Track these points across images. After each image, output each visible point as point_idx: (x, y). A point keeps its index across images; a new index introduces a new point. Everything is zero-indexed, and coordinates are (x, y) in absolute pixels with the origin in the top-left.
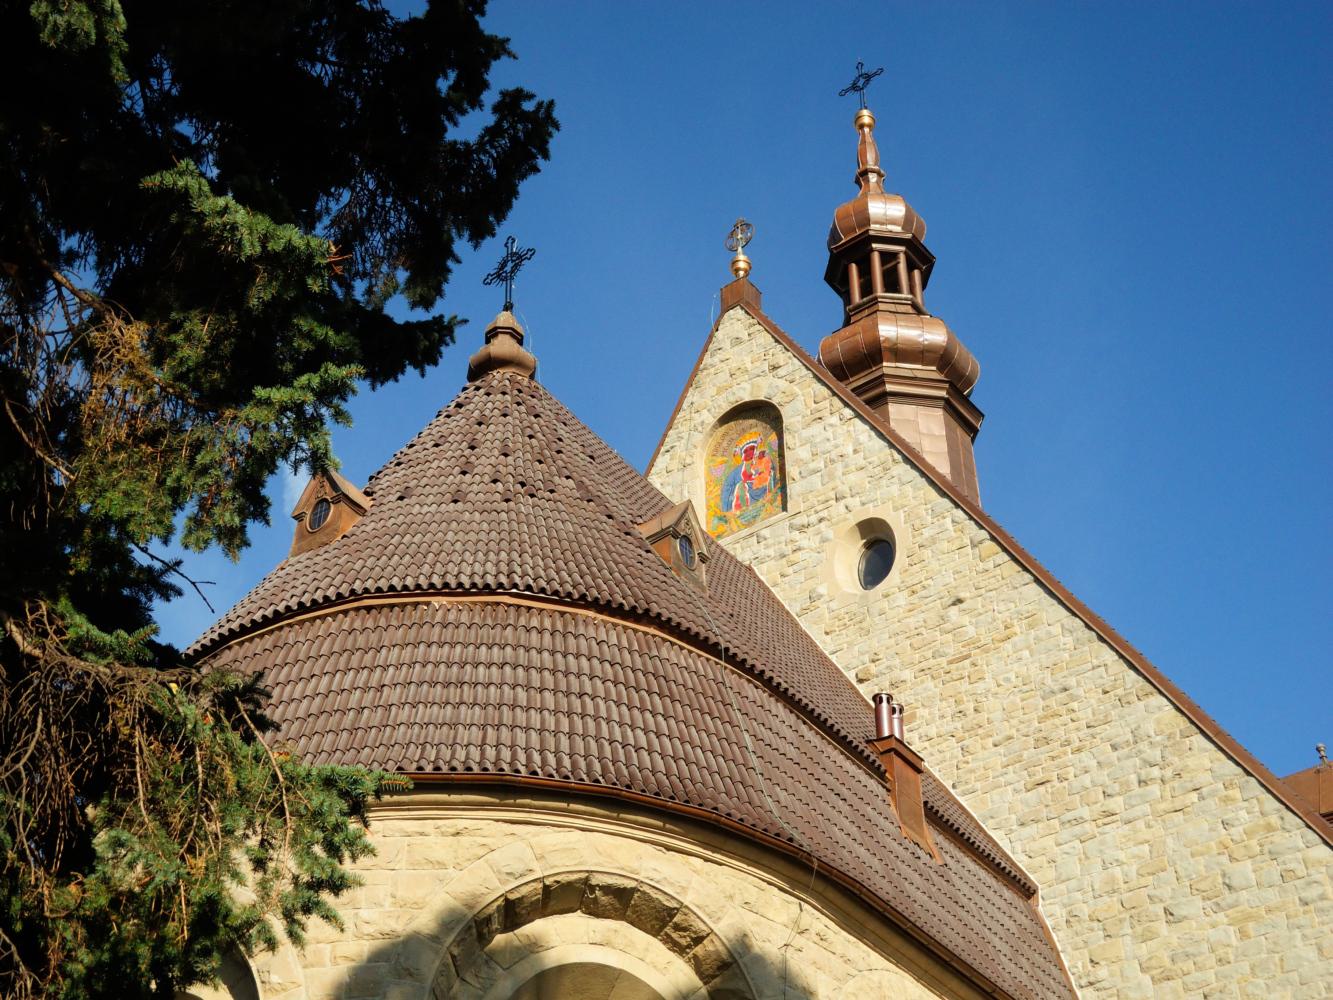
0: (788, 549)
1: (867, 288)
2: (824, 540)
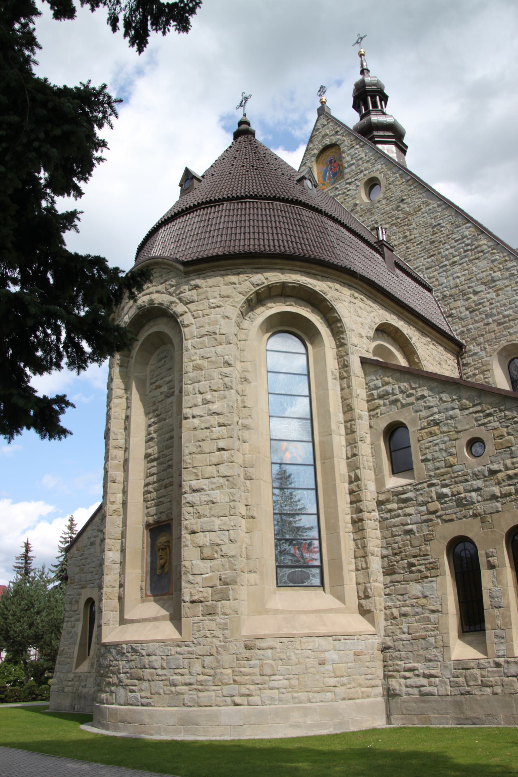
0: (345, 191)
1: (367, 108)
2: (358, 186)
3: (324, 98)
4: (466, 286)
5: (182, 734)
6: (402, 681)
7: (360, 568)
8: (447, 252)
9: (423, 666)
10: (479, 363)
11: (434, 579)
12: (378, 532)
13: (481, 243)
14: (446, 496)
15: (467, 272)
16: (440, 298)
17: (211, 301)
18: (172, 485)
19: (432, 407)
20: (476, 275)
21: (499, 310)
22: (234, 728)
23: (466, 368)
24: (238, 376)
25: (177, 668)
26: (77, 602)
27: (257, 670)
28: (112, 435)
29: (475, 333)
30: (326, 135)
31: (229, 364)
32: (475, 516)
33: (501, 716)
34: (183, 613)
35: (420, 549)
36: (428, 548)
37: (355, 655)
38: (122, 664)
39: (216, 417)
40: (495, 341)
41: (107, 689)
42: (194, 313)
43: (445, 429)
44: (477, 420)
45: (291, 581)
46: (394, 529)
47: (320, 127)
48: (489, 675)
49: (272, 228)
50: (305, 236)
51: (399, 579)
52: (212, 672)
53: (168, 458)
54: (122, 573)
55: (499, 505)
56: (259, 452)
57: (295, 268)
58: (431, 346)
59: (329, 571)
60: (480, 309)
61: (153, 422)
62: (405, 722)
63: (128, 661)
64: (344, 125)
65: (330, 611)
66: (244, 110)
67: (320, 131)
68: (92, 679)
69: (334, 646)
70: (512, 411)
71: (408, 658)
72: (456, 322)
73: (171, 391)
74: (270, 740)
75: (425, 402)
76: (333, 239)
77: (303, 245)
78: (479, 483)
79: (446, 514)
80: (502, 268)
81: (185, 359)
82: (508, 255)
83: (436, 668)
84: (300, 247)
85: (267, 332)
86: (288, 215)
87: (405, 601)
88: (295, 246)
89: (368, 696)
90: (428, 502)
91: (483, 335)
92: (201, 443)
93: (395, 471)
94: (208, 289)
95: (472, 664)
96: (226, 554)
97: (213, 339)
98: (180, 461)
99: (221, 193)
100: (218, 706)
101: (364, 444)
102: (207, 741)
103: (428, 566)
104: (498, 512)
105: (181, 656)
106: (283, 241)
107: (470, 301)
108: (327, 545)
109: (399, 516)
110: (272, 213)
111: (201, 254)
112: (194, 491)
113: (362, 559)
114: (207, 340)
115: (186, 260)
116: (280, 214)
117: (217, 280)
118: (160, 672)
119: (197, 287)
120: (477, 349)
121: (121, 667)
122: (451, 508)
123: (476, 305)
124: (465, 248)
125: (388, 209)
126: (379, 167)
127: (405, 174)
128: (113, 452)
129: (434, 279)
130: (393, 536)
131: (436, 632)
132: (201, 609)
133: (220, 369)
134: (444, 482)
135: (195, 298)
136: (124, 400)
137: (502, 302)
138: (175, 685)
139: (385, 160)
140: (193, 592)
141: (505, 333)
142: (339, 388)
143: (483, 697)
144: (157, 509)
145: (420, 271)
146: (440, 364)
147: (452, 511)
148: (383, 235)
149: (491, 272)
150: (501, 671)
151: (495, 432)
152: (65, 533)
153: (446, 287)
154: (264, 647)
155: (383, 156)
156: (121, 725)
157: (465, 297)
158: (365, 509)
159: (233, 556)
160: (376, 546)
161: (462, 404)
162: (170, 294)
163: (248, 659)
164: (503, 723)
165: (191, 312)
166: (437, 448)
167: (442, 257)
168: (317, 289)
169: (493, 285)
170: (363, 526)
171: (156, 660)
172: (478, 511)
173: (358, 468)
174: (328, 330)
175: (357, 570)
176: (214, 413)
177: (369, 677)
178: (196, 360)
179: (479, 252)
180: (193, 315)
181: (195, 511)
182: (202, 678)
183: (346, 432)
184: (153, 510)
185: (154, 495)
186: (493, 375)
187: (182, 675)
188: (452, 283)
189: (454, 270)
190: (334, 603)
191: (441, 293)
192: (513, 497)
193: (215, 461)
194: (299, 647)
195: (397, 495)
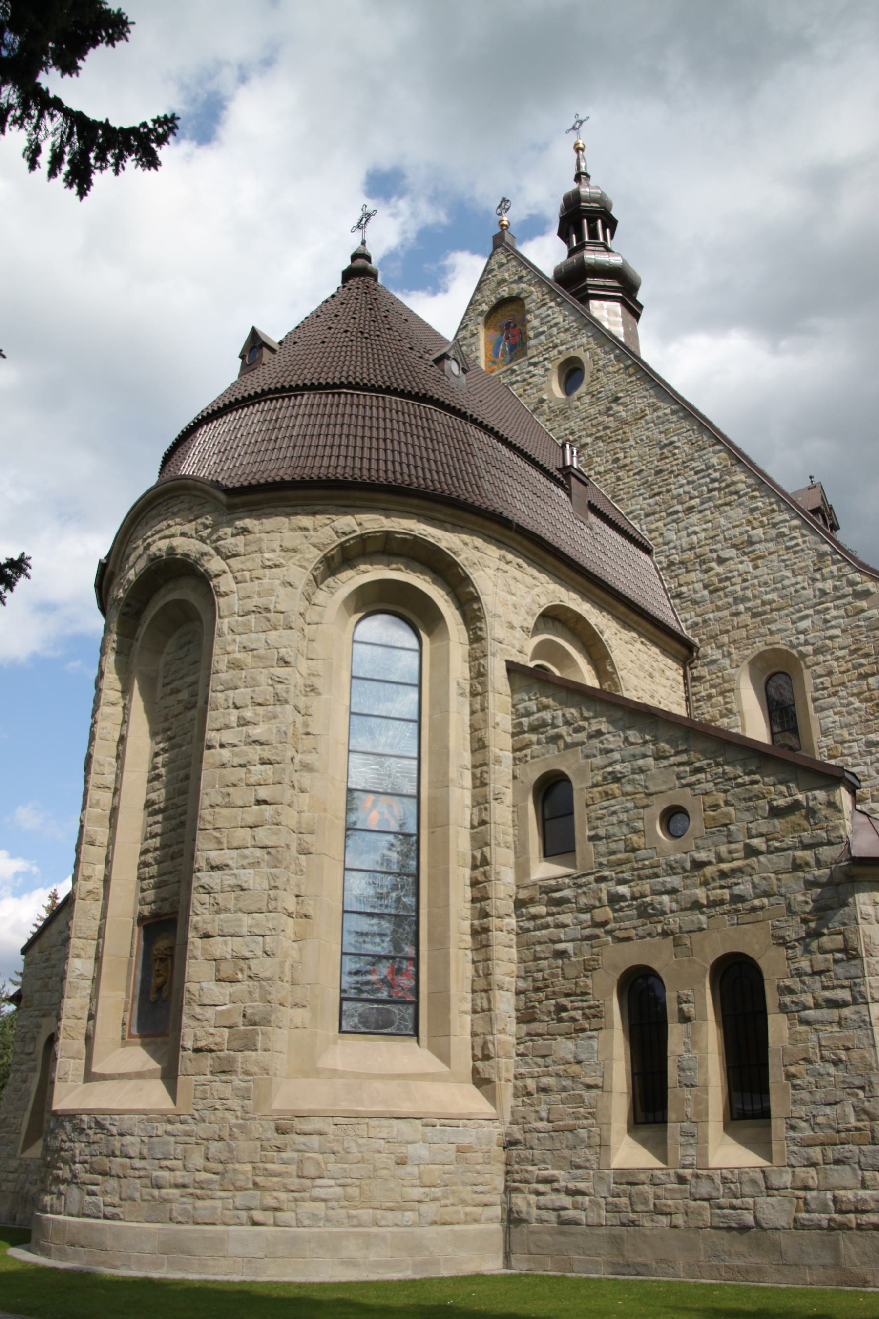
0: (527, 376)
2: (547, 370)
3: (505, 219)
4: (707, 548)
5: (165, 1268)
6: (533, 1198)
7: (479, 1009)
8: (681, 491)
9: (567, 1176)
10: (718, 677)
12: (514, 950)
13: (735, 478)
14: (622, 898)
15: (710, 524)
16: (665, 565)
17: (266, 555)
19: (612, 751)
20: (723, 531)
21: (756, 592)
22: (249, 1262)
23: (697, 684)
24: (301, 682)
25: (165, 1159)
26: (34, 1038)
27: (292, 1168)
28: (94, 766)
29: (716, 627)
30: (504, 281)
31: (286, 663)
32: (665, 934)
33: (681, 1263)
34: (181, 1068)
36: (589, 982)
38: (79, 1146)
39: (258, 748)
41: (54, 1189)
43: (629, 788)
44: (679, 778)
46: (538, 948)
47: (496, 267)
48: (667, 1196)
49: (378, 439)
50: (432, 457)
51: (540, 1031)
52: (220, 1167)
53: (180, 810)
54: (94, 996)
55: (703, 918)
56: (325, 810)
57: (408, 509)
58: (638, 646)
59: (429, 1011)
60: (725, 587)
61: (162, 749)
62: (533, 1266)
63: (89, 1143)
66: (364, 235)
67: (495, 273)
69: (424, 1135)
70: (734, 766)
71: (544, 1162)
72: (687, 607)
74: (300, 1285)
75: (602, 742)
76: (480, 463)
77: (427, 471)
78: (675, 881)
79: (620, 929)
80: (766, 522)
81: (216, 650)
82: (777, 502)
83: (586, 1180)
84: (420, 474)
85: (356, 611)
86: (407, 420)
87: (547, 1067)
89: (476, 1221)
90: (595, 907)
91: (727, 632)
92: (231, 790)
93: (549, 853)
94: (264, 536)
95: (642, 1177)
96: (257, 975)
97: (263, 620)
98: (195, 818)
99: (302, 377)
100: (225, 1224)
101: (501, 806)
102: (199, 1281)
103: (587, 1011)
104: (701, 929)
105: (172, 1139)
107: (712, 573)
108: (429, 969)
109: (547, 926)
110: (381, 415)
111: (257, 477)
112: (213, 868)
113: (483, 994)
114: (253, 621)
115: (231, 486)
116: (395, 416)
118: (137, 1163)
119: (245, 531)
120: (717, 654)
121: (77, 1152)
123: (720, 581)
125: (592, 411)
126: (584, 340)
127: (624, 356)
128: (94, 794)
129: (656, 534)
130: (537, 959)
132: (210, 1062)
133: (271, 670)
135: (241, 549)
136: (119, 709)
137: (762, 579)
138: (159, 1187)
139: (595, 330)
140: (198, 1034)
143: (655, 1232)
144: (156, 894)
145: (635, 518)
146: (651, 676)
147: (631, 924)
148: (572, 457)
149: (749, 528)
150: (685, 1191)
151: (706, 798)
153: (675, 548)
154: (307, 1131)
156: (70, 1249)
157: (704, 567)
158: (493, 913)
159: (268, 979)
160: (509, 975)
161: (658, 750)
162: (202, 540)
163: (279, 1149)
164: (682, 1274)
165: (231, 571)
166: (614, 819)
167: (673, 498)
168: (443, 545)
169: (750, 549)
170: (488, 940)
171: (133, 1144)
173: (487, 844)
174: (457, 614)
175: (474, 1011)
176: (255, 741)
177: (479, 1188)
178: (234, 652)
179: (731, 494)
180: (235, 578)
181: (212, 901)
182: (203, 1176)
183: (473, 783)
184: (150, 895)
185: (154, 869)
186: (739, 700)
187: (172, 1170)
188: (685, 541)
189: (690, 521)
191: (667, 557)
192: (726, 907)
193: (250, 820)
194: (365, 1134)
195: (547, 893)
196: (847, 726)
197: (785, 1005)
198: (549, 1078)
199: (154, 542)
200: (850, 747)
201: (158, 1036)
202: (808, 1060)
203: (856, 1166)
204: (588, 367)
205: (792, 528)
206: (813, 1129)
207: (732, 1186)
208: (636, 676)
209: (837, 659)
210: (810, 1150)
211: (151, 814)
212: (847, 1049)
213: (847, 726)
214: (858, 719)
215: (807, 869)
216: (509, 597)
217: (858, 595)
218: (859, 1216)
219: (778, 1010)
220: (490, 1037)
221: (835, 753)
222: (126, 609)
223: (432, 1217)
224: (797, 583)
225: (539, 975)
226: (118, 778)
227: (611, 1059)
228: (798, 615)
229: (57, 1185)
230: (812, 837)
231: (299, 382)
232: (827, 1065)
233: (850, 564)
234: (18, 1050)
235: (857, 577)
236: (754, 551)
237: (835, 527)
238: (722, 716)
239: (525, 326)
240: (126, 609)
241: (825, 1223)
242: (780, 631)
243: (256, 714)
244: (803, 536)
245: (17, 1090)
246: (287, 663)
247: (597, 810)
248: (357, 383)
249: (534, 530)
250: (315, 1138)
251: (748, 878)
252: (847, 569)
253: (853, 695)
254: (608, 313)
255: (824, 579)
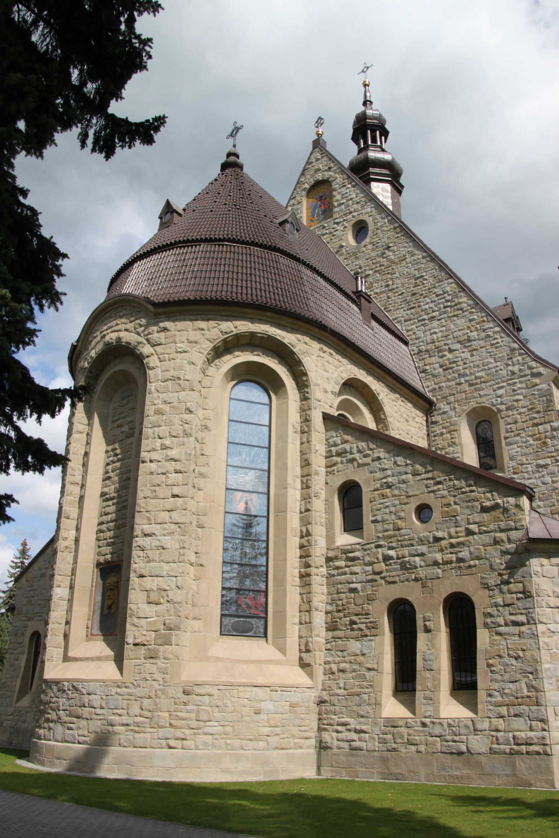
0: (333, 230)
1: (365, 142)
2: (345, 227)
3: (320, 130)
4: (442, 343)
6: (335, 735)
8: (427, 306)
9: (355, 722)
11: (373, 638)
13: (461, 300)
14: (391, 558)
15: (444, 328)
16: (416, 352)
17: (178, 345)
18: (125, 526)
19: (386, 469)
20: (453, 333)
21: (472, 371)
22: (167, 770)
24: (199, 423)
26: (23, 634)
27: (193, 715)
29: (446, 392)
30: (319, 170)
31: (190, 411)
32: (416, 580)
33: (422, 773)
34: (126, 655)
35: (362, 608)
36: (370, 607)
37: (291, 706)
38: (62, 701)
39: (173, 463)
40: (465, 401)
41: (46, 725)
42: (160, 356)
43: (396, 492)
44: (427, 487)
45: (235, 630)
46: (339, 586)
47: (314, 161)
48: (415, 734)
50: (279, 286)
51: (340, 636)
53: (123, 499)
54: (69, 610)
55: (440, 571)
56: (213, 501)
57: (265, 318)
58: (400, 402)
60: (453, 367)
62: (334, 774)
64: (338, 162)
65: (270, 662)
66: (234, 141)
67: (313, 164)
68: (32, 714)
71: (342, 713)
73: (132, 431)
75: (380, 464)
77: (276, 295)
78: (423, 549)
79: (389, 576)
81: (147, 402)
82: (486, 316)
85: (232, 380)
86: (264, 262)
88: (268, 295)
89: (301, 747)
90: (374, 563)
91: (454, 394)
92: (157, 488)
94: (177, 333)
95: (400, 723)
96: (172, 600)
97: (177, 385)
98: (134, 504)
99: (200, 234)
100: (152, 747)
103: (369, 624)
104: (438, 578)
105: (120, 697)
106: (256, 289)
109: (345, 574)
111: (173, 296)
112: (145, 535)
113: (307, 614)
114: (170, 385)
115: (157, 301)
116: (257, 260)
117: (187, 324)
118: (99, 711)
119: (165, 329)
120: (447, 408)
122: (395, 570)
123: (450, 363)
124: (445, 304)
128: (69, 488)
129: (411, 333)
131: (370, 690)
132: (143, 652)
134: (390, 544)
135: (163, 341)
136: (84, 436)
141: (475, 395)
142: (298, 442)
143: (407, 755)
145: (398, 322)
147: (396, 573)
149: (468, 331)
150: (426, 731)
151: (443, 500)
152: (17, 558)
153: (422, 341)
155: (373, 199)
156: (57, 761)
157: (440, 354)
158: (313, 565)
159: (179, 603)
160: (321, 602)
162: (138, 334)
163: (185, 704)
164: (423, 779)
166: (387, 510)
167: (422, 311)
168: (286, 341)
169: (469, 344)
172: (420, 576)
174: (293, 383)
175: (301, 623)
177: (303, 728)
178: (159, 404)
179: (458, 310)
180: (159, 358)
181: (145, 555)
182: (139, 719)
183: (302, 486)
187: (120, 715)
188: (429, 338)
189: (432, 325)
190: (275, 654)
191: (417, 347)
192: (454, 565)
193: (168, 507)
194: (236, 696)
195: (345, 553)
196: (525, 454)
197: (487, 624)
198: (345, 664)
199: (108, 334)
200: (527, 468)
201: (110, 635)
202: (500, 656)
203: (527, 718)
204: (371, 227)
205: (495, 333)
206: (502, 697)
207: (454, 729)
208: (399, 421)
209: (520, 414)
210: (500, 708)
211: (104, 501)
212: (523, 650)
213: (525, 454)
214: (532, 451)
215: (502, 544)
216: (325, 373)
217: (533, 375)
218: (528, 747)
219: (483, 626)
220: (310, 639)
221: (517, 471)
222: (89, 374)
223: (275, 745)
224: (497, 367)
225: (340, 603)
226: (84, 477)
227: (382, 653)
228: (497, 386)
229: (47, 723)
230: (506, 525)
231: (198, 237)
232: (511, 659)
233: (529, 356)
234: (12, 641)
235: (534, 364)
236: (471, 345)
237: (519, 329)
238: (449, 446)
239: (332, 199)
240: (89, 374)
241: (508, 751)
242: (486, 395)
243: (172, 443)
244: (502, 337)
245: (12, 665)
246: (191, 412)
247: (376, 505)
248: (234, 239)
249: (340, 332)
250: (207, 697)
251: (467, 548)
252: (528, 359)
253: (529, 436)
254: (382, 190)
255: (514, 365)
